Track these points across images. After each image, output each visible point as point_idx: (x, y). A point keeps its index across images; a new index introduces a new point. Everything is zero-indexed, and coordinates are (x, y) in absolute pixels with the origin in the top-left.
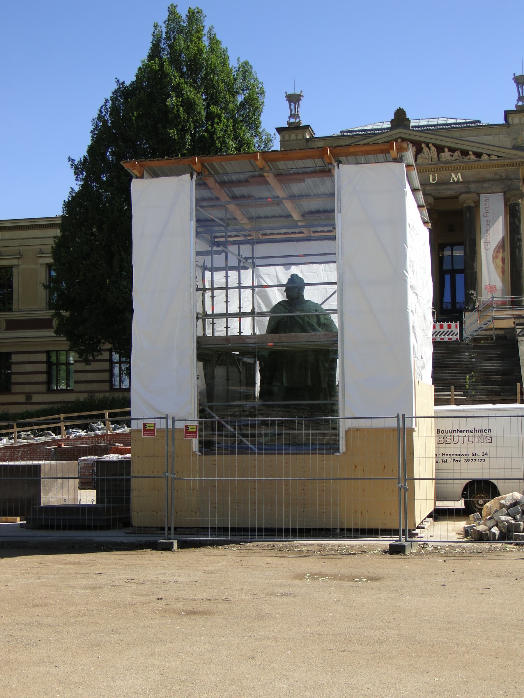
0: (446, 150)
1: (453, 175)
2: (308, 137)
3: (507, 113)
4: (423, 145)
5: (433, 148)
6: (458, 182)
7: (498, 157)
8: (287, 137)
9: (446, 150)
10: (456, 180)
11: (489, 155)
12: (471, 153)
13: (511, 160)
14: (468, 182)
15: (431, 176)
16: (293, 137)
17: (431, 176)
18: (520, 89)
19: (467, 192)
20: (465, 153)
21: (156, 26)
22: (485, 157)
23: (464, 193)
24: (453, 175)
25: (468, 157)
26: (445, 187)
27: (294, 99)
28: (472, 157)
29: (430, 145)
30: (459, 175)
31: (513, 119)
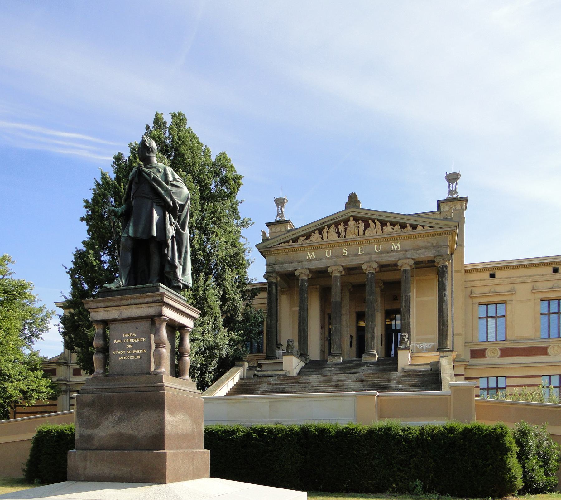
0: (388, 224)
1: (393, 244)
2: (289, 228)
3: (440, 203)
4: (370, 222)
5: (378, 223)
6: (397, 251)
7: (430, 227)
8: (274, 230)
9: (388, 224)
10: (395, 249)
11: (423, 226)
12: (408, 225)
13: (441, 230)
14: (406, 251)
15: (376, 246)
16: (278, 229)
17: (376, 246)
18: (451, 186)
19: (404, 258)
20: (403, 226)
21: (148, 127)
22: (419, 228)
23: (402, 259)
24: (393, 244)
25: (406, 229)
26: (387, 254)
27: (280, 202)
28: (409, 228)
29: (376, 221)
30: (399, 244)
31: (444, 207)
